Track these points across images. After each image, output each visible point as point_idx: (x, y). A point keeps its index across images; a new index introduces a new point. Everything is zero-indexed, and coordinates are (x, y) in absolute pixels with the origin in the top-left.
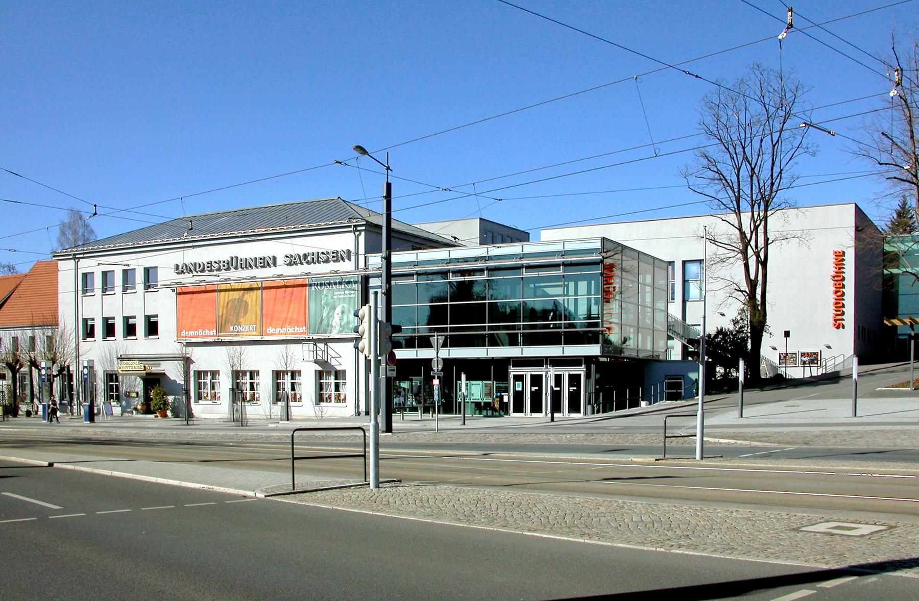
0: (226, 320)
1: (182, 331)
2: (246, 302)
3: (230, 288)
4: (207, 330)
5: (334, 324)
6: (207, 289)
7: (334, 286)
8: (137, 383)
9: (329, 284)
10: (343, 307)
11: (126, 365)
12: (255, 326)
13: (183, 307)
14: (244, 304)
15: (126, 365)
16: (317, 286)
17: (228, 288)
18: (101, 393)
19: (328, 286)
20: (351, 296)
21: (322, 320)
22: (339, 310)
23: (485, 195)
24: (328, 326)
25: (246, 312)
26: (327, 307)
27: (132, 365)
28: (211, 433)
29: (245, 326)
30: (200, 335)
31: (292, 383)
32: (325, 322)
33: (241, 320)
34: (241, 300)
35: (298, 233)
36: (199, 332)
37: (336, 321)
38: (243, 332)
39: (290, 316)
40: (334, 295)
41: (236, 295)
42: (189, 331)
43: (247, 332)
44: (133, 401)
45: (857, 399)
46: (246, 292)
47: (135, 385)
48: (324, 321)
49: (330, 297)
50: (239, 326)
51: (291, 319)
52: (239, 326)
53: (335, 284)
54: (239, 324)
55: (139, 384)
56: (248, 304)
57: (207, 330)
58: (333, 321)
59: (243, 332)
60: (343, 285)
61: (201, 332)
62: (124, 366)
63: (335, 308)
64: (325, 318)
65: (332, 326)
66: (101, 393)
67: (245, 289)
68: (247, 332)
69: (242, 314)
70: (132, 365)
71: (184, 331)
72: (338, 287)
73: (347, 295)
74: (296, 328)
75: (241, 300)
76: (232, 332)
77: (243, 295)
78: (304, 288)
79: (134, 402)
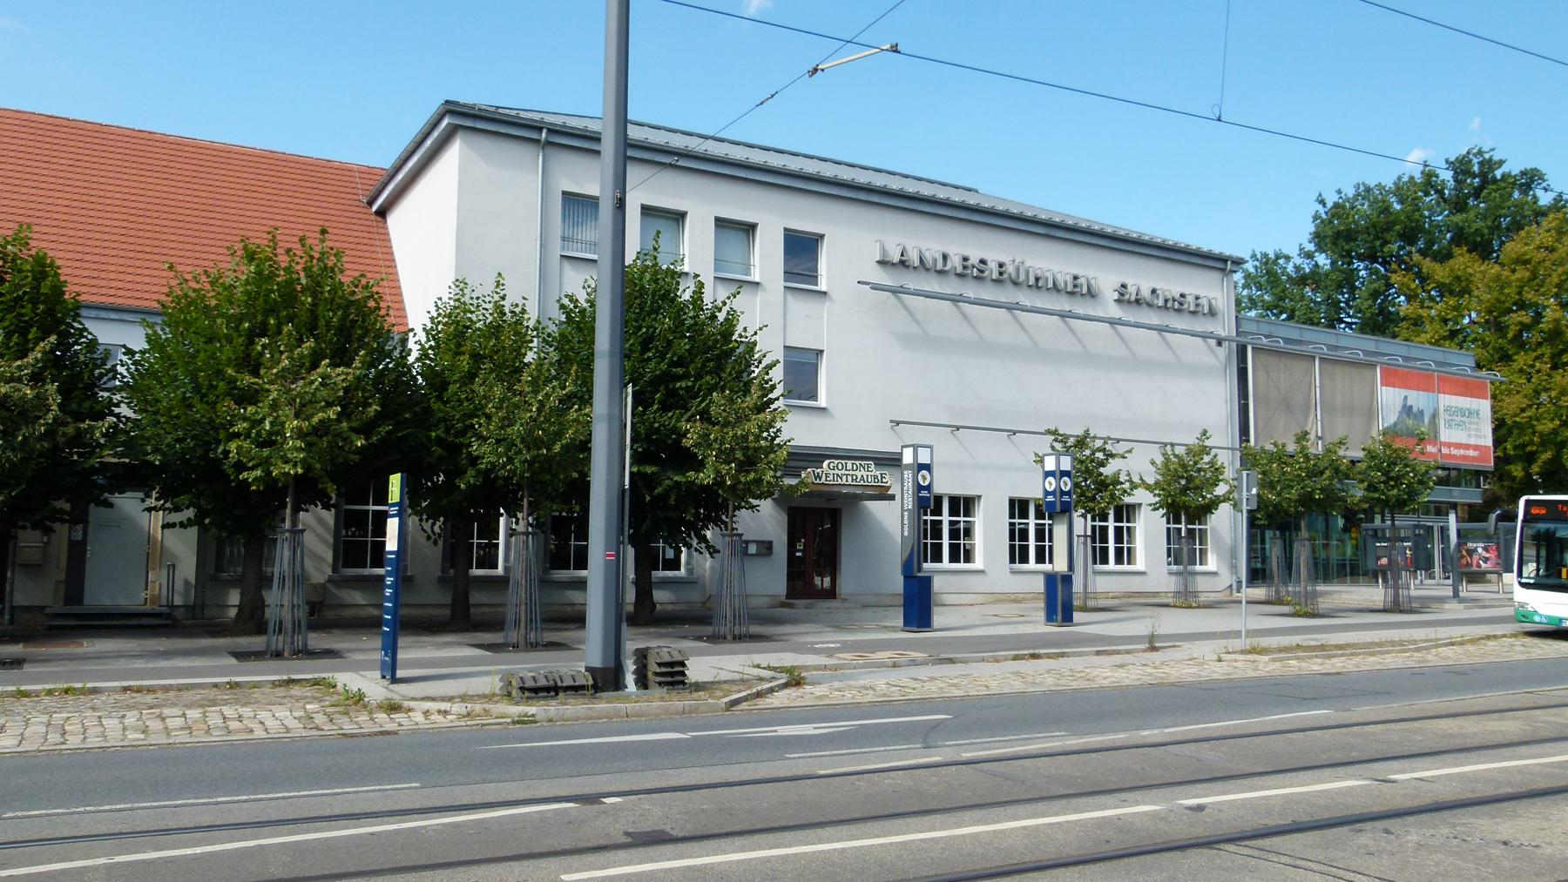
11: (836, 472)
15: (836, 472)
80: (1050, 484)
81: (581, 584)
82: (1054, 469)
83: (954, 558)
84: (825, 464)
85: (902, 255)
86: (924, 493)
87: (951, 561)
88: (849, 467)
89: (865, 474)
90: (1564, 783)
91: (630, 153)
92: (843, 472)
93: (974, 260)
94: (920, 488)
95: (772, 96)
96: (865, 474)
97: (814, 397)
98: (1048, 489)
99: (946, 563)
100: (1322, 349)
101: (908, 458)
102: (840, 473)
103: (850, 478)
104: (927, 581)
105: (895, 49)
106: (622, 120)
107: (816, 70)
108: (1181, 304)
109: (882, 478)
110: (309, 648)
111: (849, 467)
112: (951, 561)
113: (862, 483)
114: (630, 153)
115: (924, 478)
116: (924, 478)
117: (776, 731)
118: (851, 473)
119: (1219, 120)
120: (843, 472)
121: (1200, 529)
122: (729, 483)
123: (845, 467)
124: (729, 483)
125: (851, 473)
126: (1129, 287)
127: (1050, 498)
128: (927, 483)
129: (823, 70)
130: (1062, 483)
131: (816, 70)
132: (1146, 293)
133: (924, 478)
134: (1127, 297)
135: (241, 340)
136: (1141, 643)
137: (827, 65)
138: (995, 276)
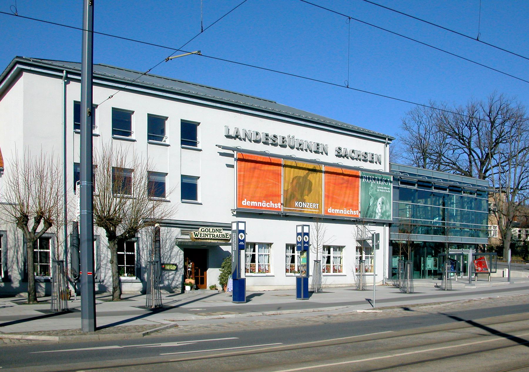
0: (291, 196)
1: (242, 199)
2: (311, 183)
3: (295, 165)
4: (271, 202)
5: (377, 211)
6: (272, 162)
7: (389, 183)
8: (173, 253)
9: (374, 179)
10: (383, 199)
11: (205, 233)
12: (317, 204)
13: (244, 174)
14: (308, 183)
15: (205, 233)
16: (366, 179)
17: (293, 165)
18: (106, 264)
19: (374, 181)
20: (388, 191)
21: (369, 207)
22: (380, 200)
23: (14, 14)
24: (373, 213)
25: (310, 190)
26: (373, 197)
27: (215, 233)
28: (19, 337)
29: (309, 204)
30: (263, 206)
31: (330, 254)
32: (371, 209)
33: (306, 197)
34: (305, 177)
35: (367, 136)
36: (263, 203)
37: (378, 210)
38: (308, 208)
39: (346, 200)
40: (377, 189)
41: (302, 173)
42: (251, 201)
43: (311, 209)
44: (166, 275)
45: (97, 318)
46: (310, 172)
47: (170, 256)
48: (370, 208)
49: (375, 189)
50: (303, 203)
51: (347, 203)
52: (303, 203)
53: (378, 180)
54: (304, 201)
55: (177, 255)
56: (312, 183)
57: (271, 202)
58: (377, 209)
59: (308, 208)
60: (364, 179)
61: (265, 203)
62: (203, 233)
63: (377, 199)
64: (372, 206)
65: (376, 213)
66: (106, 264)
67: (309, 170)
68: (311, 209)
69: (306, 192)
70: (215, 233)
71: (245, 200)
72: (380, 183)
73: (385, 190)
74: (351, 211)
75: (305, 177)
76: (297, 207)
77: (308, 175)
78: (358, 179)
79: (169, 275)
80: (299, 238)
82: (301, 232)
84: (200, 229)
85: (237, 133)
86: (242, 243)
88: (211, 230)
91: (94, 81)
92: (208, 233)
93: (271, 135)
94: (240, 241)
95: (150, 70)
97: (196, 199)
101: (234, 227)
103: (211, 236)
104: (243, 281)
105: (199, 53)
106: (91, 64)
107: (168, 60)
108: (365, 157)
109: (226, 235)
111: (211, 230)
113: (217, 238)
114: (94, 81)
115: (241, 236)
116: (242, 236)
117: (178, 343)
118: (212, 233)
120: (208, 233)
123: (209, 231)
125: (212, 233)
126: (342, 150)
127: (299, 245)
128: (243, 238)
129: (171, 59)
130: (304, 238)
131: (168, 60)
132: (349, 152)
133: (242, 236)
134: (340, 154)
136: (52, 276)
137: (174, 57)
138: (281, 143)
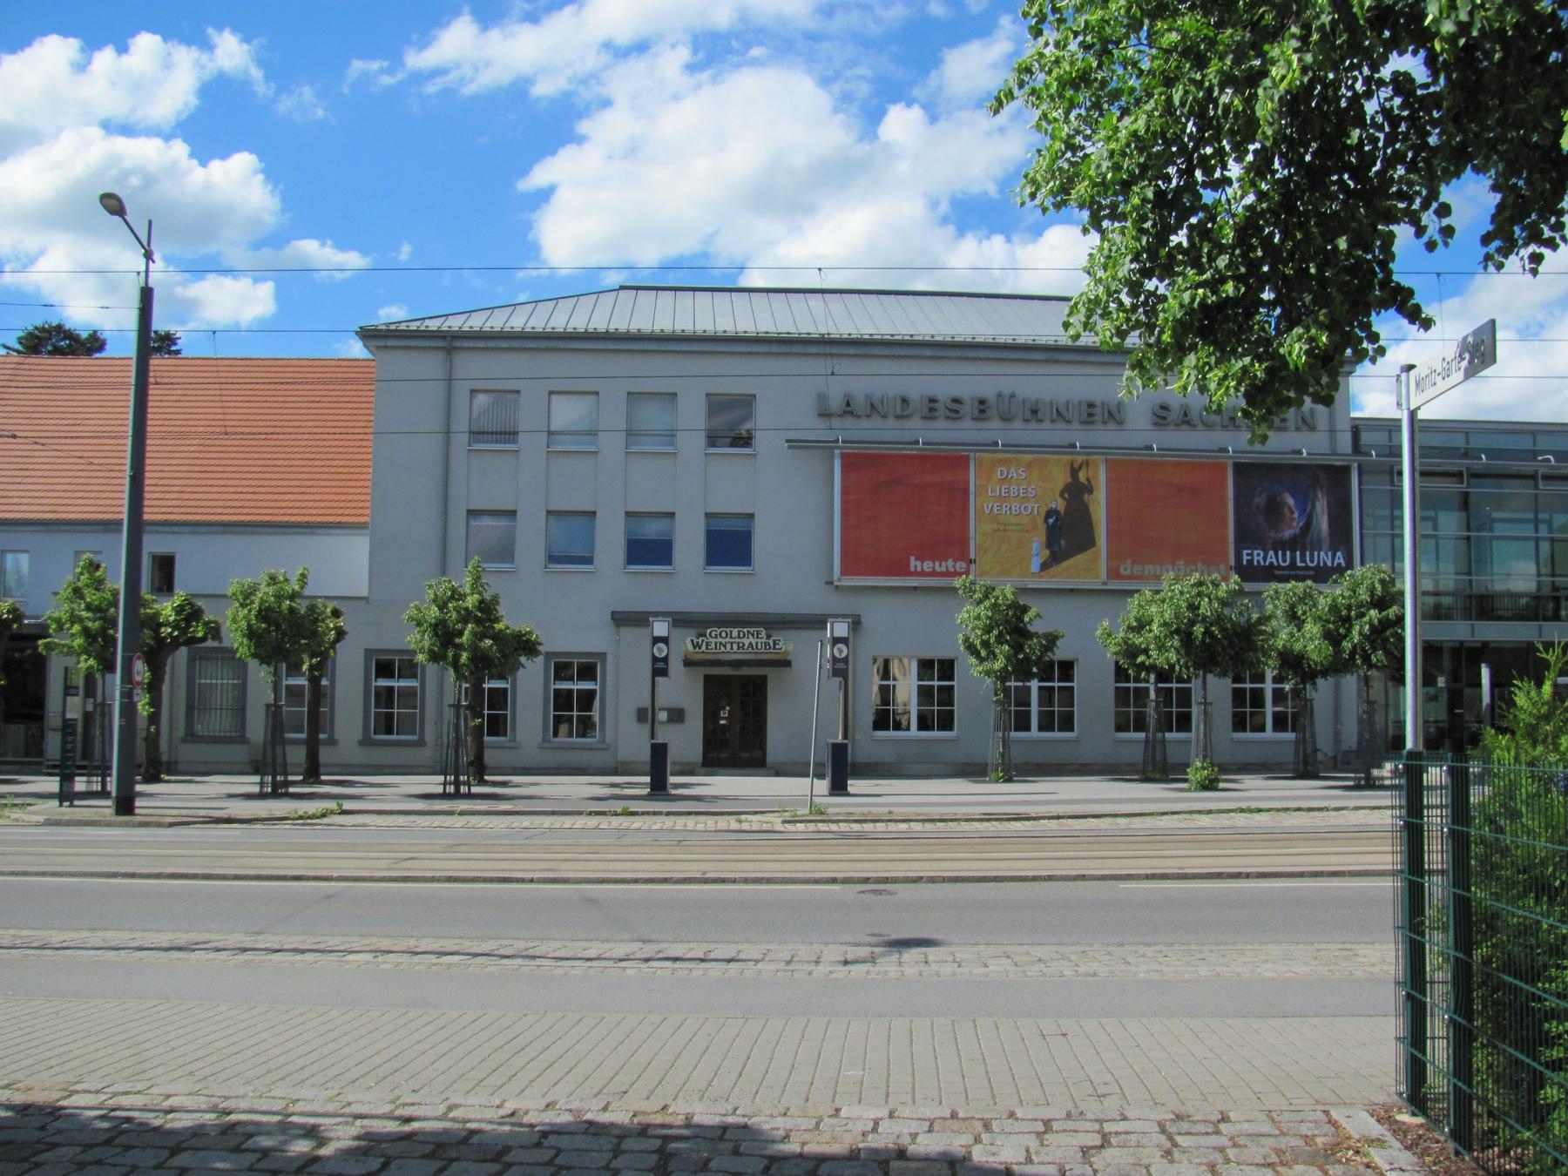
11: (719, 640)
15: (719, 640)
81: (570, 735)
83: (1045, 725)
87: (1041, 729)
89: (754, 641)
90: (3, 528)
92: (728, 640)
96: (754, 641)
98: (657, 655)
99: (1035, 731)
100: (1549, 460)
102: (723, 641)
110: (1392, 312)
112: (1041, 729)
119: (820, 269)
120: (728, 640)
121: (1136, 689)
122: (1510, 33)
124: (1510, 33)
128: (663, 655)
135: (1508, 841)
